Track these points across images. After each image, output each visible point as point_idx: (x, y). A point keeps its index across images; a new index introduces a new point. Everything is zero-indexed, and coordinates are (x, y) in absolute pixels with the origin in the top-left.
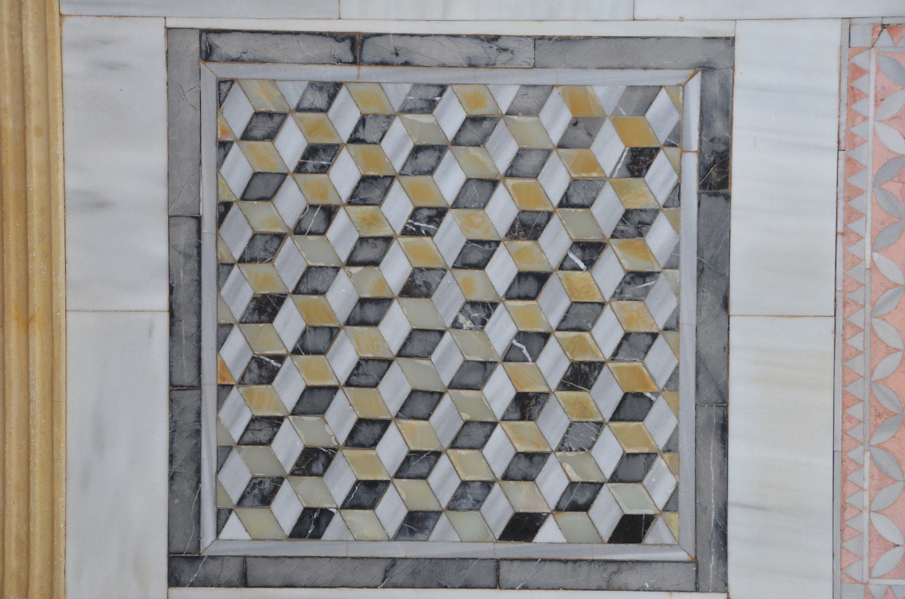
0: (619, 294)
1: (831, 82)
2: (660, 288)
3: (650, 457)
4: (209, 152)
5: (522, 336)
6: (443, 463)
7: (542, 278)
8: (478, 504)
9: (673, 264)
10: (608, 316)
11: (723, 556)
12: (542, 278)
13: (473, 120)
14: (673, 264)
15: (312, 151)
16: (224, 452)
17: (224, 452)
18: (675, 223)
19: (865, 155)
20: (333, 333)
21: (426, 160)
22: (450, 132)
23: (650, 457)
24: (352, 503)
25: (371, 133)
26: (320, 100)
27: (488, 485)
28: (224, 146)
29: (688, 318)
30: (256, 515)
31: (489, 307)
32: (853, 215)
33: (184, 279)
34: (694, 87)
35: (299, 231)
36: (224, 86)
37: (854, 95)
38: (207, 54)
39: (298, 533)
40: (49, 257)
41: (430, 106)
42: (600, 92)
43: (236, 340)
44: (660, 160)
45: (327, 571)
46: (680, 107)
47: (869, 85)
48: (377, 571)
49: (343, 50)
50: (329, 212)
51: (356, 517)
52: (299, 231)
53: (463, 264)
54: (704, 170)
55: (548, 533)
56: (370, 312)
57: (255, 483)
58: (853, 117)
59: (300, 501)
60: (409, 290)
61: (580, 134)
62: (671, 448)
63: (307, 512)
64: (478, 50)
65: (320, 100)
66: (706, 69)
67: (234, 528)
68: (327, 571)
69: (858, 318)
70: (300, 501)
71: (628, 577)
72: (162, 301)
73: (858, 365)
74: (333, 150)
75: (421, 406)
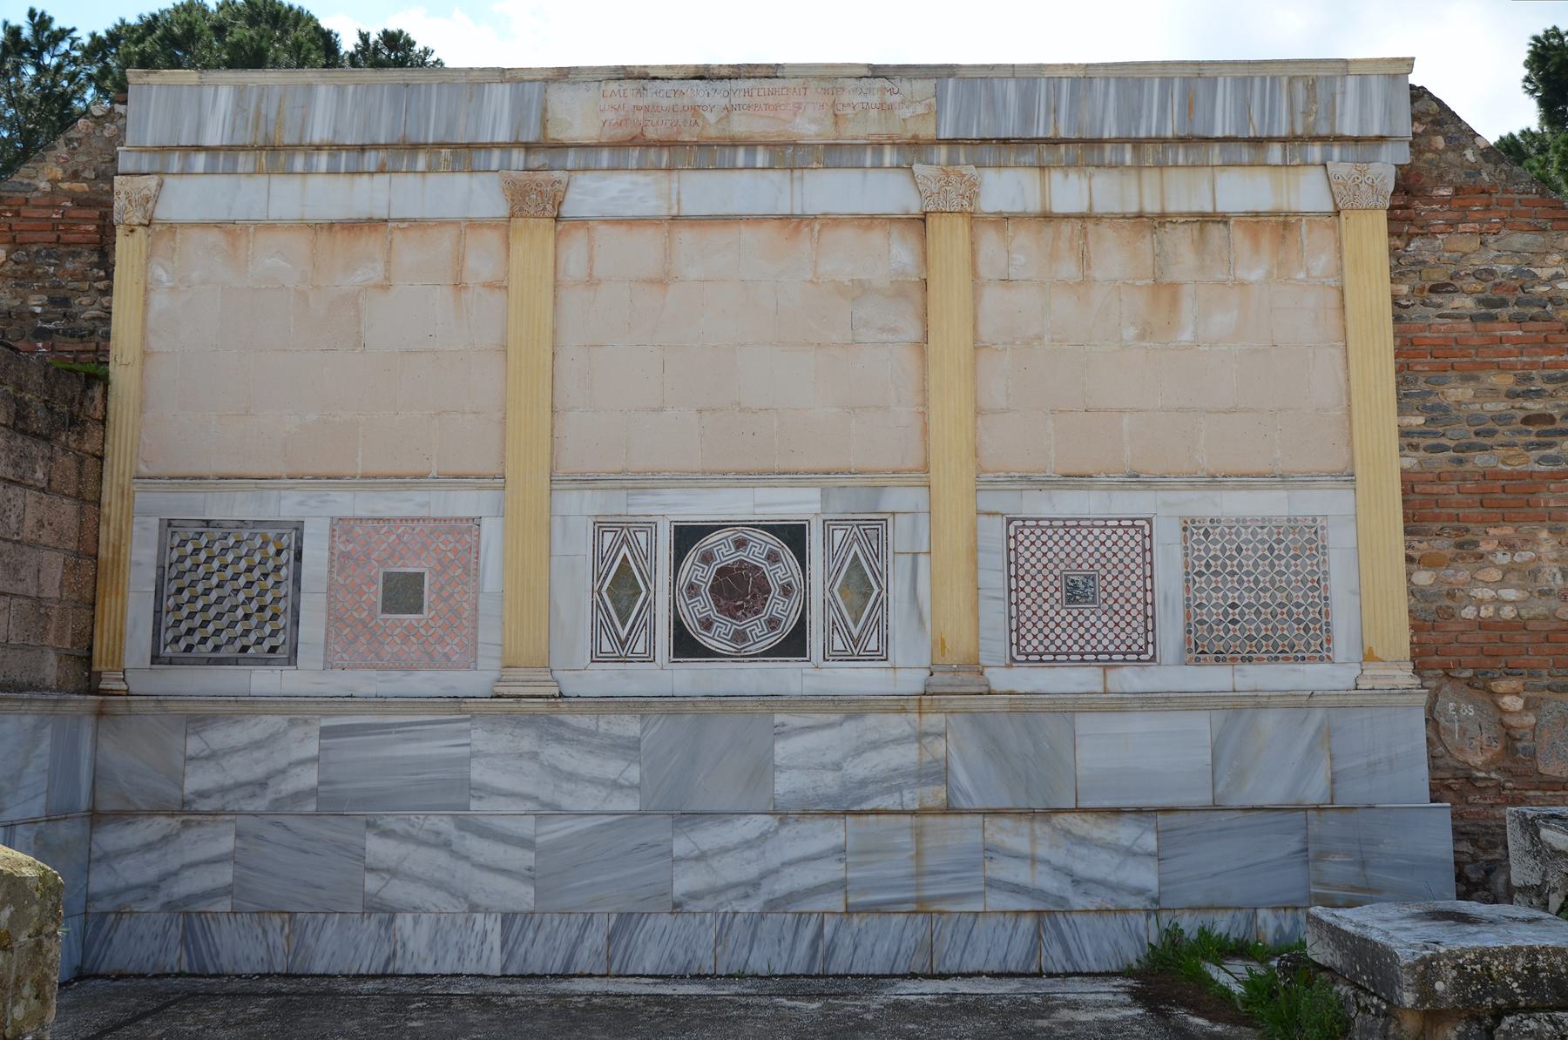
0: (272, 587)
1: (327, 532)
2: (283, 585)
3: (279, 630)
4: (168, 550)
5: (246, 598)
6: (224, 632)
7: (253, 583)
8: (233, 643)
9: (287, 579)
10: (269, 593)
11: (296, 656)
12: (253, 583)
13: (237, 542)
14: (287, 579)
15: (194, 550)
16: (167, 629)
17: (167, 629)
18: (288, 568)
19: (337, 553)
20: (197, 597)
21: (224, 552)
22: (231, 545)
23: (279, 630)
24: (199, 643)
25: (210, 545)
26: (197, 537)
27: (236, 638)
28: (172, 549)
29: (290, 593)
30: (174, 646)
31: (238, 591)
32: (332, 566)
33: (159, 583)
34: (294, 534)
35: (190, 571)
36: (173, 533)
37: (333, 536)
38: (169, 525)
39: (185, 651)
40: (121, 641)
41: (226, 538)
42: (270, 534)
43: (172, 599)
44: (284, 552)
45: (192, 661)
46: (290, 538)
47: (337, 533)
48: (205, 661)
49: (204, 524)
50: (198, 566)
51: (201, 646)
52: (190, 571)
53: (232, 579)
54: (295, 555)
55: (251, 651)
56: (207, 592)
57: (174, 637)
58: (333, 542)
59: (1026, 694)
60: (218, 586)
61: (264, 545)
62: (284, 628)
63: (188, 645)
64: (239, 523)
65: (197, 537)
66: (297, 529)
67: (168, 649)
68: (192, 661)
69: (333, 594)
70: (1026, 694)
71: (272, 662)
72: (154, 589)
73: (332, 605)
74: (201, 549)
75: (219, 617)
